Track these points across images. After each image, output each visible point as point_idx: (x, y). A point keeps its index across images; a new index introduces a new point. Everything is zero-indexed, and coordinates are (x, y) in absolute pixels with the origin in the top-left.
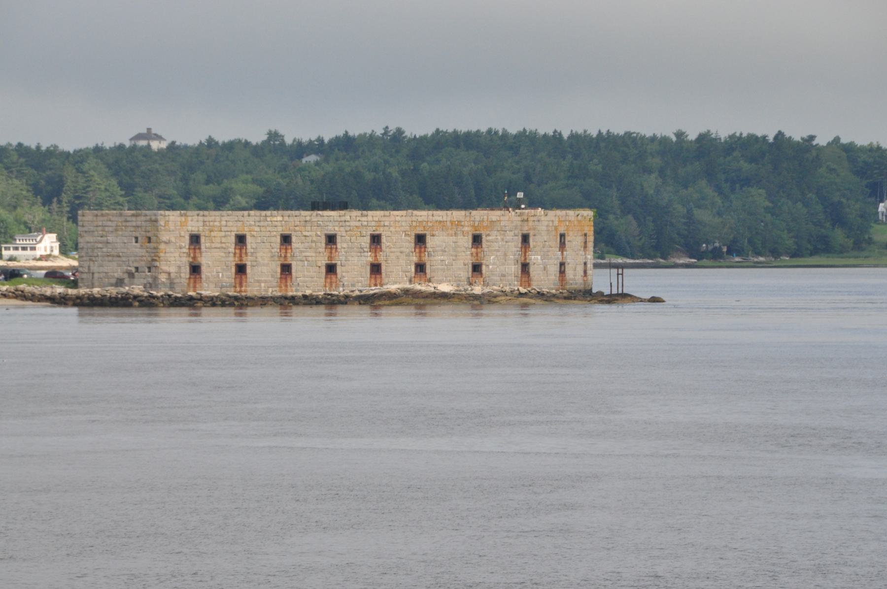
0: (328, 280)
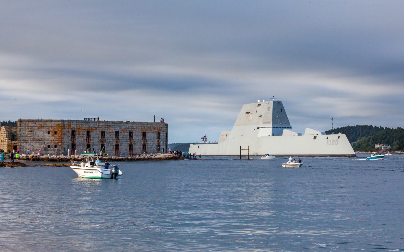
0: (116, 152)
